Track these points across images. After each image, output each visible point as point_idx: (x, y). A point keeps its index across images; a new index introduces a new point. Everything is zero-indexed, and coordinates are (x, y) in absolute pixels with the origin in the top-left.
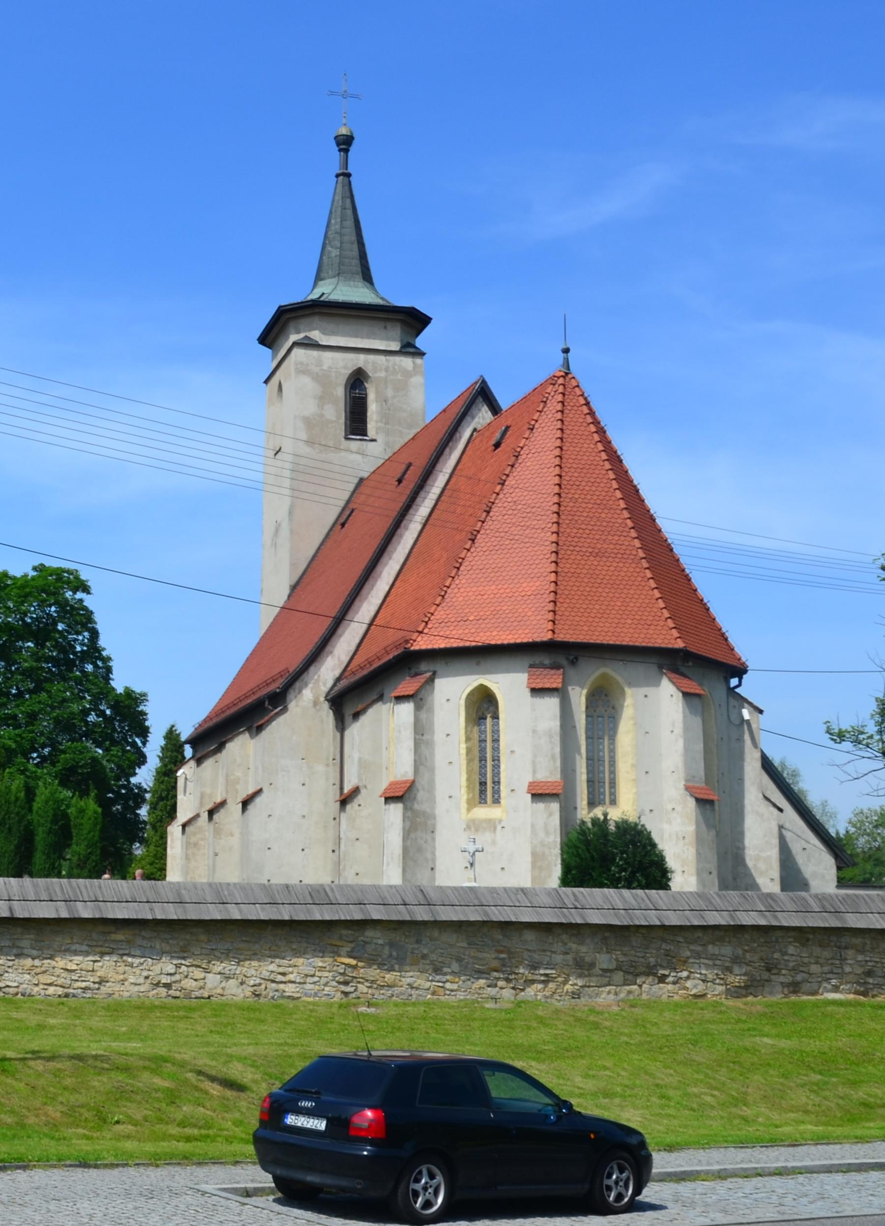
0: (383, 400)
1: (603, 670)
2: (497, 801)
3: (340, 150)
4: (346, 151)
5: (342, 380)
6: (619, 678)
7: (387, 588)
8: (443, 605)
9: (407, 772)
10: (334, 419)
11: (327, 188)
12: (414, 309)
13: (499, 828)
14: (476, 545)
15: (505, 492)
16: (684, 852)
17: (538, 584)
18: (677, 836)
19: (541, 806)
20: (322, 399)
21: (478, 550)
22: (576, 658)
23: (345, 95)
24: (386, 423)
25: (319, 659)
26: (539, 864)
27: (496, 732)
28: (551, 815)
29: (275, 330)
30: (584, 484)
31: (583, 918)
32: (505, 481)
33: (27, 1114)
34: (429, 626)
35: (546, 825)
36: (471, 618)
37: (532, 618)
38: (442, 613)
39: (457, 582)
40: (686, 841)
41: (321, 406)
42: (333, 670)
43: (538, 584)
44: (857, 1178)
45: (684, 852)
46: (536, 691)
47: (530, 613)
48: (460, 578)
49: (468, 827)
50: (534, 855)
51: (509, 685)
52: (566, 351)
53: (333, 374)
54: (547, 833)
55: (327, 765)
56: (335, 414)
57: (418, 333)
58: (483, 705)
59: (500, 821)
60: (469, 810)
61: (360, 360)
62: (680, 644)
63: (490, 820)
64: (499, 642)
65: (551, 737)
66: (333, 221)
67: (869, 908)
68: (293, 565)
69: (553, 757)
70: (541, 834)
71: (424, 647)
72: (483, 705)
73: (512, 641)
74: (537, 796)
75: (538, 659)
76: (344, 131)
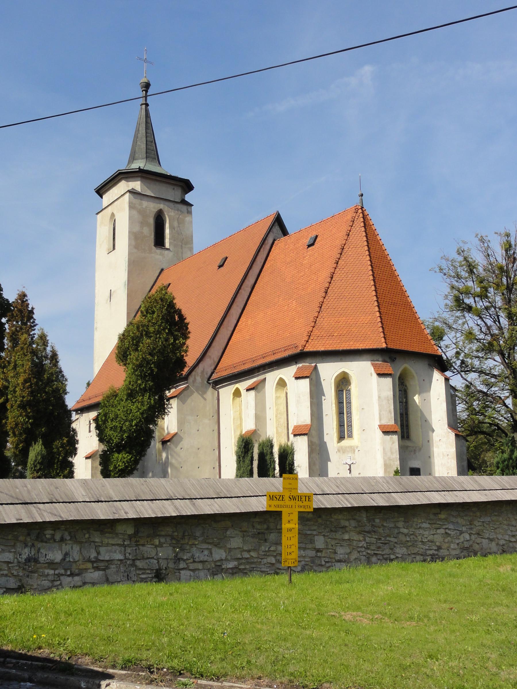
0: (171, 228)
1: (406, 365)
2: (350, 436)
7: (235, 322)
8: (316, 327)
9: (306, 420)
10: (148, 235)
12: (188, 180)
13: (357, 451)
14: (329, 295)
15: (339, 267)
16: (448, 463)
17: (370, 317)
18: (443, 454)
19: (388, 437)
20: (143, 223)
21: (330, 298)
22: (395, 358)
23: (145, 61)
24: (174, 241)
25: (204, 360)
26: (388, 470)
28: (393, 443)
29: (154, 177)
31: (429, 500)
32: (338, 262)
34: (311, 338)
35: (391, 449)
36: (335, 335)
37: (371, 335)
39: (322, 315)
40: (450, 456)
42: (211, 366)
43: (370, 317)
46: (380, 375)
47: (369, 333)
49: (339, 451)
52: (362, 195)
53: (148, 211)
54: (392, 453)
55: (210, 419)
56: (149, 232)
57: (187, 193)
59: (357, 447)
60: (338, 442)
61: (161, 206)
63: (351, 447)
64: (356, 348)
65: (388, 400)
66: (140, 129)
67: (424, 495)
69: (390, 411)
70: (389, 454)
71: (311, 350)
72: (343, 382)
73: (363, 348)
76: (145, 80)
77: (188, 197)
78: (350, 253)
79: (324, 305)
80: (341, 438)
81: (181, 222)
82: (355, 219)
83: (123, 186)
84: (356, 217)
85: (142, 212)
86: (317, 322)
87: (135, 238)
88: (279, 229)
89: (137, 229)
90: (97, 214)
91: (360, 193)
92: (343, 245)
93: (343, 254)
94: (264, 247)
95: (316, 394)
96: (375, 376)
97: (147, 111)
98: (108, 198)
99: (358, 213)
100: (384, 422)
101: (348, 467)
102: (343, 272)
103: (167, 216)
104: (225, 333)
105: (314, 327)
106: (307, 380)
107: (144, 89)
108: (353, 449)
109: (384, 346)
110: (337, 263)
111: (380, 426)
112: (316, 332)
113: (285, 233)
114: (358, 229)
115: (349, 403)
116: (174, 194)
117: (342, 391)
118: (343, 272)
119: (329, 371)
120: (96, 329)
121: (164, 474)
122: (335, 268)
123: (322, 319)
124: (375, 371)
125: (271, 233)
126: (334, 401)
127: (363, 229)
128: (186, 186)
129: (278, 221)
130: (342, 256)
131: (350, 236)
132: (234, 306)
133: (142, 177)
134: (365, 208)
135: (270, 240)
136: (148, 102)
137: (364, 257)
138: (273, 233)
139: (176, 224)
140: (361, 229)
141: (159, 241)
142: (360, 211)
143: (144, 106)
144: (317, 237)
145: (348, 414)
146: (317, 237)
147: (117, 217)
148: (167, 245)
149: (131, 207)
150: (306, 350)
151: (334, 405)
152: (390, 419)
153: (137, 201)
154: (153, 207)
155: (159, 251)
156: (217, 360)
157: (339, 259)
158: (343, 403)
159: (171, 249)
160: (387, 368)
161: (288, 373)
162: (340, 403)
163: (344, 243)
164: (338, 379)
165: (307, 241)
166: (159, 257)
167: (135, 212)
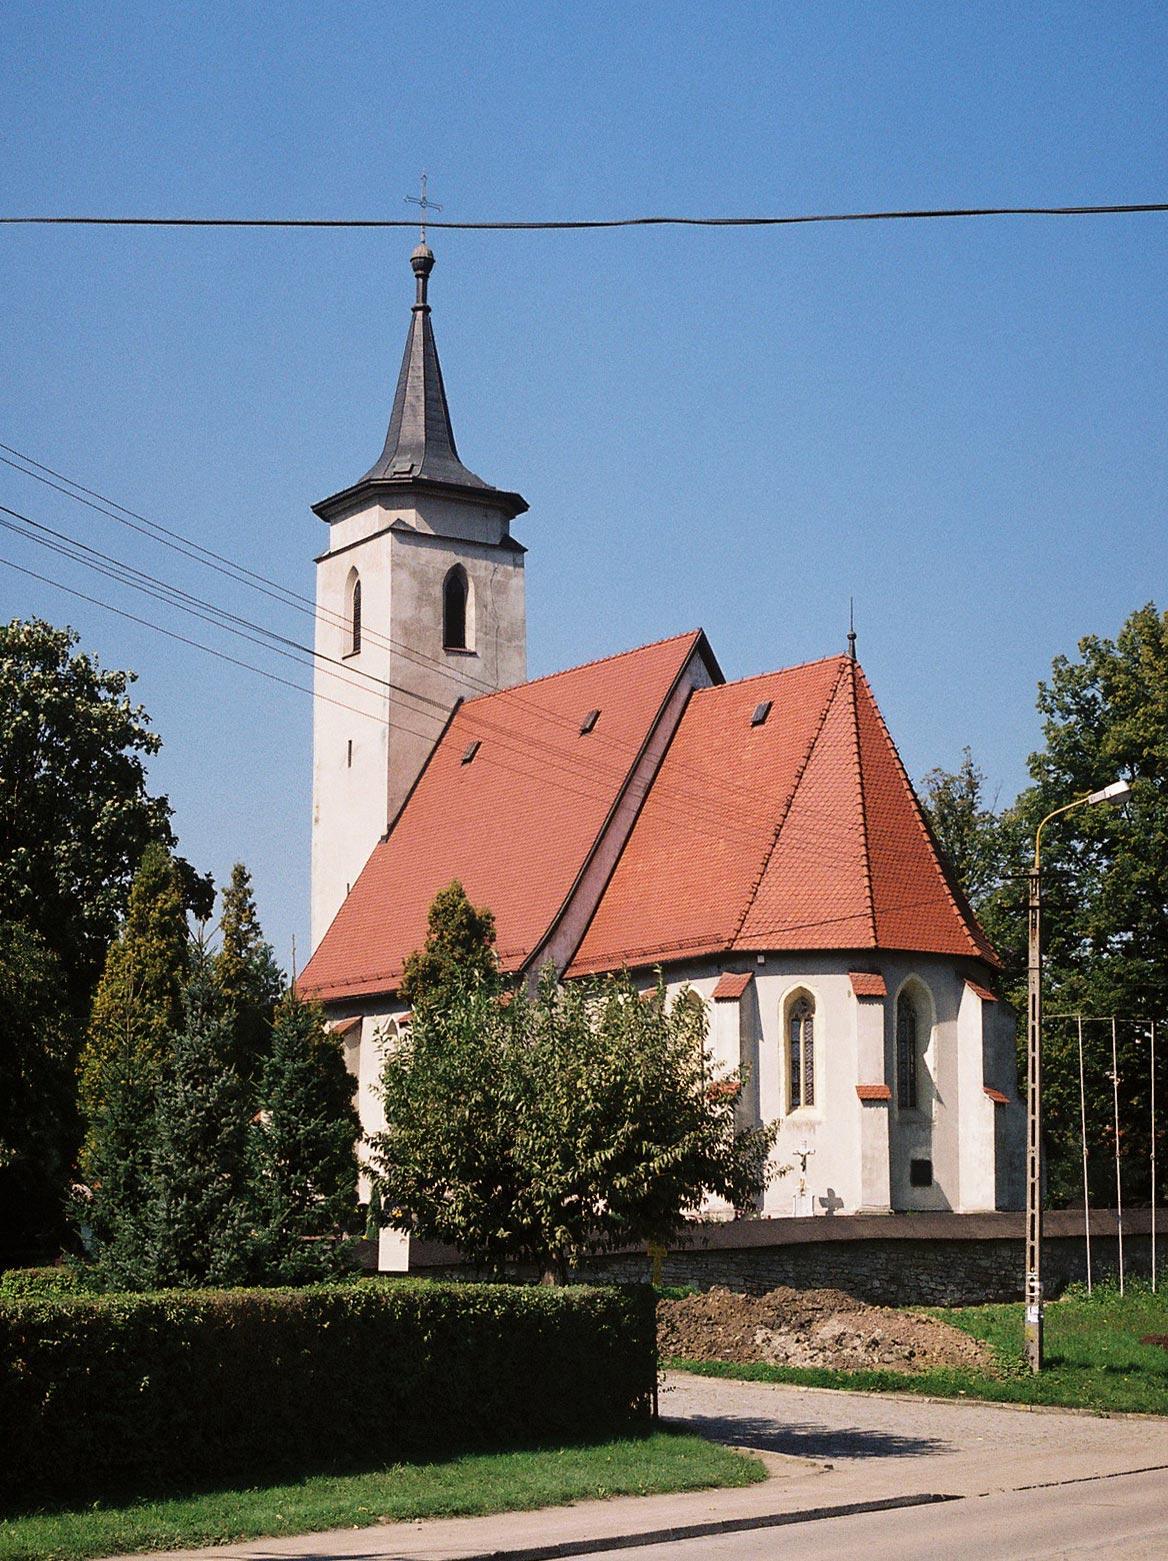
0: (481, 604)
2: (810, 1101)
3: (417, 276)
4: (425, 277)
5: (440, 579)
6: (925, 986)
11: (400, 322)
12: (518, 496)
14: (781, 841)
20: (421, 599)
27: (809, 1034)
30: (880, 783)
32: (802, 774)
33: (195, 1482)
34: (746, 925)
38: (757, 911)
39: (767, 879)
41: (419, 607)
44: (716, 1505)
45: (981, 1152)
46: (863, 998)
48: (770, 875)
50: (864, 1157)
51: (832, 991)
52: (853, 637)
56: (432, 618)
58: (800, 1009)
62: (977, 952)
68: (391, 801)
72: (800, 1009)
74: (867, 1102)
75: (858, 963)
77: (518, 528)
78: (825, 758)
79: (772, 860)
80: (794, 1104)
81: (501, 589)
82: (839, 687)
83: (374, 517)
84: (841, 683)
85: (418, 575)
86: (769, 865)
87: (405, 633)
88: (702, 665)
89: (408, 613)
90: (318, 560)
91: (849, 633)
92: (813, 740)
93: (812, 758)
94: (674, 702)
95: (751, 1030)
96: (854, 996)
97: (427, 324)
98: (342, 532)
99: (845, 674)
100: (868, 1082)
101: (801, 1159)
102: (810, 795)
103: (470, 579)
104: (593, 886)
105: (751, 903)
106: (737, 1004)
107: (420, 272)
108: (812, 1126)
109: (872, 944)
110: (801, 778)
111: (859, 1088)
112: (754, 913)
113: (717, 678)
114: (841, 707)
115: (809, 1043)
116: (483, 529)
117: (800, 1021)
118: (810, 795)
119: (775, 991)
120: (317, 821)
121: (244, 868)
122: (797, 788)
123: (767, 889)
124: (854, 989)
125: (687, 675)
126: (782, 1041)
127: (851, 708)
128: (514, 505)
129: (702, 648)
130: (810, 762)
131: (826, 722)
132: (612, 831)
133: (416, 494)
134: (859, 662)
135: (683, 692)
136: (428, 303)
137: (851, 766)
138: (691, 673)
139: (488, 595)
140: (848, 707)
141: (454, 638)
142: (849, 670)
143: (420, 313)
144: (770, 704)
145: (807, 1063)
146: (770, 704)
147: (362, 577)
148: (470, 644)
149: (397, 565)
150: (737, 947)
151: (782, 1048)
152: (874, 1073)
153: (407, 549)
154: (441, 560)
155: (453, 660)
156: (576, 939)
157: (804, 768)
158: (799, 1042)
159: (479, 654)
160: (875, 984)
161: (704, 987)
162: (793, 1043)
163: (815, 735)
164: (791, 1001)
165: (753, 712)
166: (455, 677)
167: (403, 575)
